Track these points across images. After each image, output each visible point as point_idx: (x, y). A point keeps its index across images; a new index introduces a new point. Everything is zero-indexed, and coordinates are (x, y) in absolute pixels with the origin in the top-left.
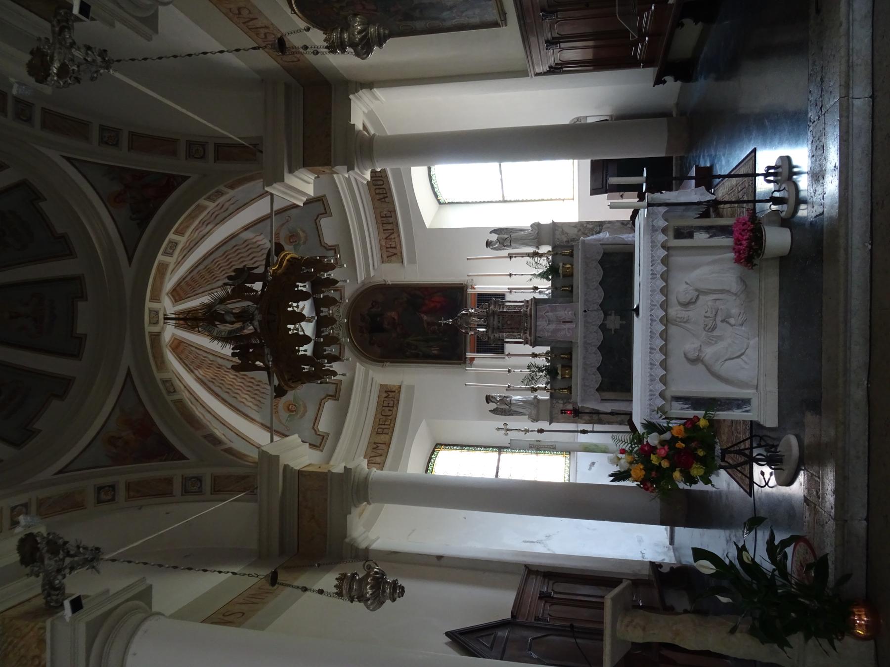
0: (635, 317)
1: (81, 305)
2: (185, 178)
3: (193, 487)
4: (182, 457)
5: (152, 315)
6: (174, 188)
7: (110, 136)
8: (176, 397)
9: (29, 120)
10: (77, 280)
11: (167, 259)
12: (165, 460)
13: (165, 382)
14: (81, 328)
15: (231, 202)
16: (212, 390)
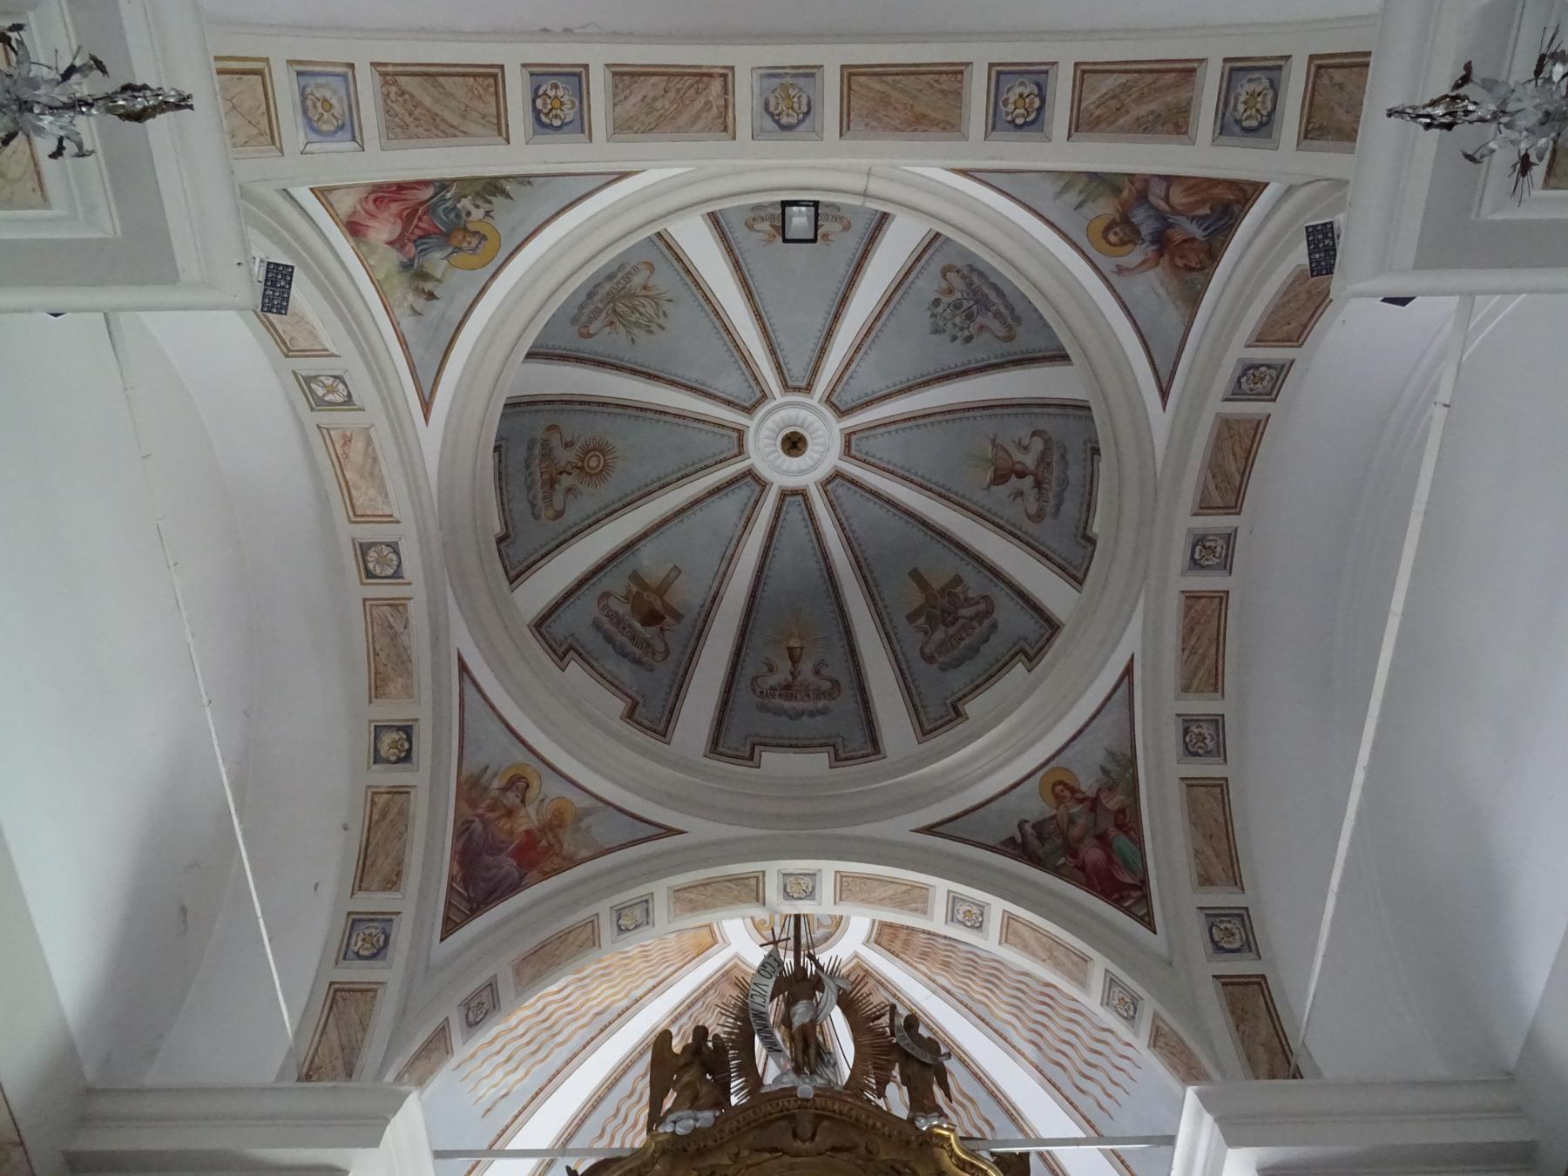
1: (822, 759)
2: (1148, 922)
3: (365, 937)
4: (450, 926)
5: (805, 881)
6: (1117, 903)
7: (1205, 737)
8: (607, 930)
9: (1236, 394)
10: (874, 745)
11: (939, 907)
12: (451, 888)
13: (646, 902)
14: (772, 761)
15: (1105, 1101)
16: (625, 1072)
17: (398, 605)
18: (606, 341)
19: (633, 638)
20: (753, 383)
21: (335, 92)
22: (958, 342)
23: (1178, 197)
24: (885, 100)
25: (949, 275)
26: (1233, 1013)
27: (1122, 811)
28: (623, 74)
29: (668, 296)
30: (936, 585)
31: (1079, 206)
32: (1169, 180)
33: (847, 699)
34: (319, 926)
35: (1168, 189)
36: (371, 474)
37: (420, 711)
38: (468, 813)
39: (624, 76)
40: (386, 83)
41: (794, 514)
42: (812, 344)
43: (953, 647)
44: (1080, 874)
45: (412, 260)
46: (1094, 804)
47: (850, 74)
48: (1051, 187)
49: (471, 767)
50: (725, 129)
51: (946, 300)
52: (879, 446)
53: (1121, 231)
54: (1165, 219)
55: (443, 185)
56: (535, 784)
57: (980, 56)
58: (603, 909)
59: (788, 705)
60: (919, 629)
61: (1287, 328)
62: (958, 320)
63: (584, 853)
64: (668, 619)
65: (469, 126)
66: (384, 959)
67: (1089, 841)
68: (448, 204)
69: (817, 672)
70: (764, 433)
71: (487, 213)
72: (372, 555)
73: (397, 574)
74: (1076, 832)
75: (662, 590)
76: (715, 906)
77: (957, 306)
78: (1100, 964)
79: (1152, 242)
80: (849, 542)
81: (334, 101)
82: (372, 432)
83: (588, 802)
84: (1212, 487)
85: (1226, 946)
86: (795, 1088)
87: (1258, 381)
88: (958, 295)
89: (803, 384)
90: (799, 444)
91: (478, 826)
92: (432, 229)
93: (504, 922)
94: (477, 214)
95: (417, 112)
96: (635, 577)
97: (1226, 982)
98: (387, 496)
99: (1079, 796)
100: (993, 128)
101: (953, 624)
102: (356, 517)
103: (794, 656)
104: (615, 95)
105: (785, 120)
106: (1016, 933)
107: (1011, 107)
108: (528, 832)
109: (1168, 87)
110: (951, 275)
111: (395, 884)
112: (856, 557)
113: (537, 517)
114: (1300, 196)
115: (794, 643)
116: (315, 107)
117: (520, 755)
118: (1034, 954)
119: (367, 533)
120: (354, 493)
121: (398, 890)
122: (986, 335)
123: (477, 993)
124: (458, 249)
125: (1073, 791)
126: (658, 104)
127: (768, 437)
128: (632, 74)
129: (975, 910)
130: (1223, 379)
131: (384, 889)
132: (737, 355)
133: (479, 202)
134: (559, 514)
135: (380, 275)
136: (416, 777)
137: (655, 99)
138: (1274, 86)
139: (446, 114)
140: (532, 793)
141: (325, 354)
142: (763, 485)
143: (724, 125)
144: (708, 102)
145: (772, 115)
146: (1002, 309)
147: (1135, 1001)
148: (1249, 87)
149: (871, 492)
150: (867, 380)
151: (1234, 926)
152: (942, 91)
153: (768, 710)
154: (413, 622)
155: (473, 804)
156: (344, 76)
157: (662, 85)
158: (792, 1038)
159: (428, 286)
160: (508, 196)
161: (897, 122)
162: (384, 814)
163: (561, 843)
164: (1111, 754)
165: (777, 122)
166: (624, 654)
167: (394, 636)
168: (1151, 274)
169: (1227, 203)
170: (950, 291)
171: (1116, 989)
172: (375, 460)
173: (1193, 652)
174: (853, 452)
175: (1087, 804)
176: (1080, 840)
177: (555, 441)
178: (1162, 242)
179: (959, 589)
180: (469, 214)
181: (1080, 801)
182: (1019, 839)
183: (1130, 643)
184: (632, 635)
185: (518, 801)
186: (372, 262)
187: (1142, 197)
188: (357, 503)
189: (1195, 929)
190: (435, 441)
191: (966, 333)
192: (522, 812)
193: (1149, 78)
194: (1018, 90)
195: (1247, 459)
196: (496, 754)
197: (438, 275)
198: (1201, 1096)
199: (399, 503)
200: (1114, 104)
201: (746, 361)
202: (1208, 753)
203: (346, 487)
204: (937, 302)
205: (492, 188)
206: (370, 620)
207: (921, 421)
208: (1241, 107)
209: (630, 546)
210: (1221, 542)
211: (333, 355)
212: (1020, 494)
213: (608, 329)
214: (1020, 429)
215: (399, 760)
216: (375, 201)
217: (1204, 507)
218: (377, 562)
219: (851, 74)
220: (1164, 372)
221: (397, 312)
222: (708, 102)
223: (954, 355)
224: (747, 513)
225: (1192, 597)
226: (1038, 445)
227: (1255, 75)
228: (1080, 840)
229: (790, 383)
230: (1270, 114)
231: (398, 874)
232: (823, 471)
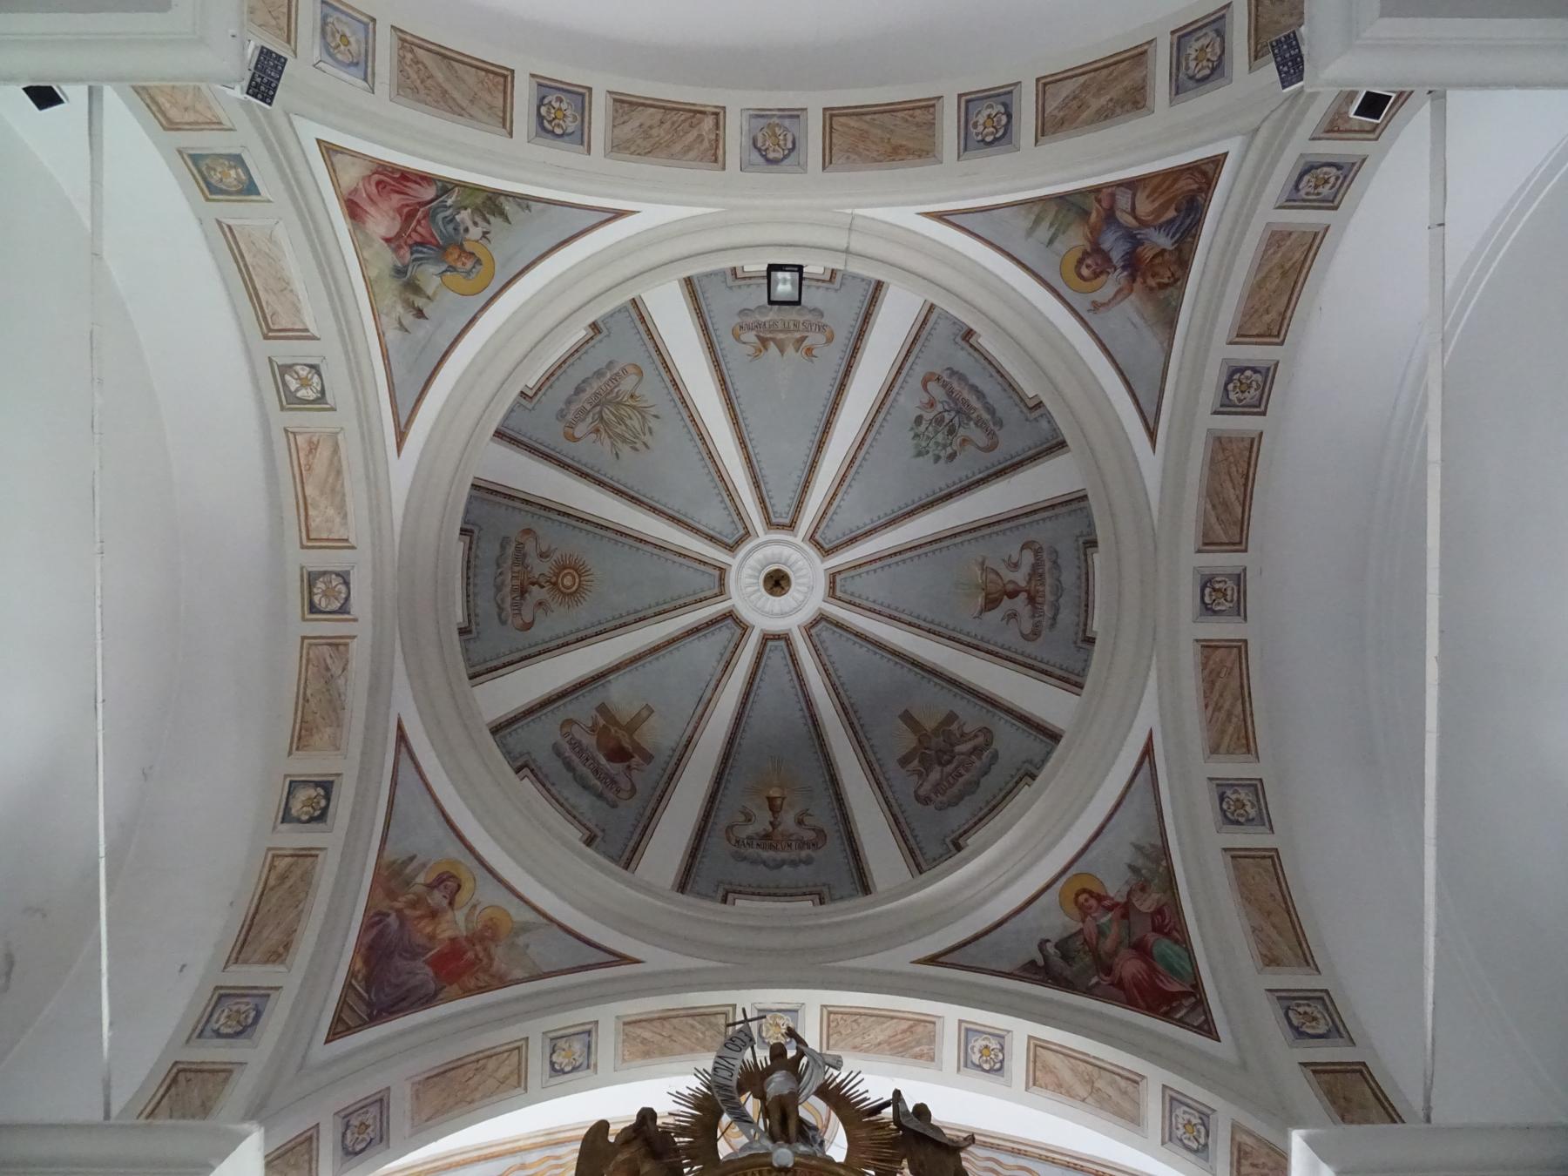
0: (615, 1129)
3: (232, 1012)
4: (339, 1029)
6: (1167, 1016)
7: (1241, 804)
12: (348, 986)
13: (588, 1033)
17: (338, 645)
18: (592, 450)
19: (596, 772)
20: (736, 518)
21: (354, 33)
22: (942, 461)
23: (1145, 207)
24: (863, 136)
25: (930, 386)
26: (1333, 1103)
27: (1159, 911)
28: (623, 102)
29: (653, 411)
30: (930, 725)
31: (1051, 241)
32: (1132, 185)
33: (834, 845)
34: (174, 1005)
35: (1134, 196)
36: (333, 490)
37: (343, 764)
38: (384, 905)
39: (624, 104)
40: (403, 47)
41: (776, 658)
42: (796, 477)
43: (951, 785)
44: (1114, 990)
45: (406, 266)
46: (1125, 910)
47: (831, 114)
48: (1023, 222)
49: (394, 852)
50: (716, 161)
51: (929, 415)
52: (866, 586)
53: (1094, 261)
54: (1133, 237)
55: (446, 186)
56: (467, 886)
57: (949, 91)
58: (535, 1030)
59: (765, 854)
60: (914, 771)
61: (1267, 318)
62: (940, 437)
63: (518, 973)
64: (637, 759)
65: (474, 110)
66: (249, 1037)
67: (1124, 952)
68: (448, 213)
69: (800, 822)
70: (746, 571)
71: (485, 234)
72: (320, 586)
73: (343, 609)
74: (1107, 944)
75: (633, 726)
76: (672, 1053)
77: (939, 421)
78: (1156, 1077)
79: (1124, 268)
80: (835, 688)
81: (352, 40)
82: (340, 437)
83: (531, 916)
84: (1213, 520)
85: (1310, 1031)
86: (768, 1154)
87: (1247, 389)
88: (939, 408)
89: (787, 521)
90: (781, 586)
91: (393, 920)
92: (432, 234)
93: (402, 1034)
94: (475, 233)
95: (429, 82)
96: (603, 709)
97: (1317, 1070)
98: (345, 516)
99: (1107, 903)
100: (966, 149)
101: (949, 762)
102: (310, 540)
103: (773, 806)
104: (614, 118)
105: (771, 155)
106: (1048, 1070)
107: (980, 128)
108: (453, 940)
109: (1124, 73)
110: (931, 386)
111: (280, 955)
112: (842, 704)
113: (503, 622)
114: (1264, 133)
115: (774, 793)
116: (333, 35)
117: (453, 850)
118: (1070, 1094)
119: (318, 560)
120: (311, 512)
121: (283, 962)
122: (970, 448)
123: (363, 1107)
124: (452, 269)
125: (1100, 898)
126: (654, 132)
127: (751, 576)
128: (631, 103)
129: (994, 1044)
130: (1209, 395)
131: (266, 962)
132: (720, 485)
133: (478, 219)
134: (528, 626)
135: (373, 273)
136: (329, 839)
137: (651, 127)
138: (1220, 34)
139: (456, 95)
140: (463, 897)
141: (304, 335)
142: (745, 628)
143: (714, 156)
144: (700, 136)
145: (759, 150)
146: (986, 416)
147: (1205, 1117)
148: (1197, 45)
149: (857, 634)
150: (851, 515)
151: (1315, 1009)
152: (918, 125)
153: (744, 859)
154: (353, 665)
155: (391, 895)
156: (366, 25)
157: (659, 116)
158: (766, 1112)
159: (419, 302)
160: (507, 220)
161: (875, 154)
162: (283, 878)
163: (491, 959)
164: (1138, 848)
165: (764, 157)
166: (586, 787)
167: (329, 680)
168: (1126, 304)
169: (1187, 193)
170: (932, 404)
171: (1180, 1111)
172: (339, 473)
173: (1218, 708)
174: (838, 594)
175: (1118, 911)
176: (1114, 953)
177: (530, 547)
178: (1133, 265)
179: (954, 727)
180: (467, 230)
181: (1110, 909)
182: (1041, 962)
183: (1147, 718)
184: (600, 768)
185: (445, 903)
186: (366, 254)
187: (1110, 217)
188: (313, 525)
189: (1269, 1019)
190: (409, 472)
191: (949, 450)
192: (449, 916)
193: (1105, 72)
194: (986, 113)
195: (1245, 485)
196: (426, 845)
197: (430, 292)
198: (1311, 1142)
199: (358, 527)
200: (1075, 104)
201: (730, 494)
202: (1250, 821)
203: (304, 504)
204: (919, 420)
205: (491, 204)
206: (306, 661)
207: (909, 554)
208: (1192, 64)
209: (600, 677)
210: (1230, 584)
211: (313, 338)
212: (1013, 615)
213: (594, 436)
214: (1010, 546)
215: (312, 820)
216: (378, 183)
217: (1208, 543)
218: (322, 594)
219: (832, 116)
220: (1150, 410)
221: (384, 319)
222: (700, 136)
223: (939, 477)
224: (727, 655)
225: (1208, 647)
226: (1028, 558)
227: (1200, 34)
228: (1114, 953)
229: (774, 520)
230: (1220, 58)
231: (287, 946)
232: (806, 615)
